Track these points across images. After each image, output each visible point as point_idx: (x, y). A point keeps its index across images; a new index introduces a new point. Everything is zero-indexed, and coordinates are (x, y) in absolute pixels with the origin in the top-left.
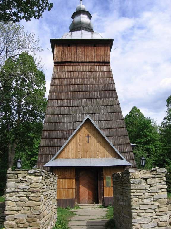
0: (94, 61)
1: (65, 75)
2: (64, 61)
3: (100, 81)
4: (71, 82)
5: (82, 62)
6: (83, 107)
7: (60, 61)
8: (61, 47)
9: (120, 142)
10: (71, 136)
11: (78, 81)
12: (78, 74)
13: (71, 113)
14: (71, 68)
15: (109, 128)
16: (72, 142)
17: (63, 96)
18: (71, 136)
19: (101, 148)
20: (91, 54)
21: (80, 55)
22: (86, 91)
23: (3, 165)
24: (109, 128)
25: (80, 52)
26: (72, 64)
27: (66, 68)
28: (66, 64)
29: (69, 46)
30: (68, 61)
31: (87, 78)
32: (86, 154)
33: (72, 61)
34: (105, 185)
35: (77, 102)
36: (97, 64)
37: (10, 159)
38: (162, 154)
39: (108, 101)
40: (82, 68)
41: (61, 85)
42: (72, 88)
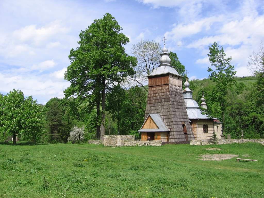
1: (152, 92)
2: (152, 86)
3: (165, 93)
7: (150, 86)
9: (169, 121)
11: (157, 95)
12: (157, 91)
13: (154, 109)
16: (146, 123)
17: (151, 102)
19: (193, 118)
20: (162, 79)
21: (157, 82)
26: (155, 87)
27: (153, 89)
28: (153, 87)
32: (150, 127)
34: (155, 138)
36: (164, 85)
37: (28, 142)
38: (58, 135)
39: (167, 103)
40: (159, 88)
41: (151, 97)
42: (154, 98)
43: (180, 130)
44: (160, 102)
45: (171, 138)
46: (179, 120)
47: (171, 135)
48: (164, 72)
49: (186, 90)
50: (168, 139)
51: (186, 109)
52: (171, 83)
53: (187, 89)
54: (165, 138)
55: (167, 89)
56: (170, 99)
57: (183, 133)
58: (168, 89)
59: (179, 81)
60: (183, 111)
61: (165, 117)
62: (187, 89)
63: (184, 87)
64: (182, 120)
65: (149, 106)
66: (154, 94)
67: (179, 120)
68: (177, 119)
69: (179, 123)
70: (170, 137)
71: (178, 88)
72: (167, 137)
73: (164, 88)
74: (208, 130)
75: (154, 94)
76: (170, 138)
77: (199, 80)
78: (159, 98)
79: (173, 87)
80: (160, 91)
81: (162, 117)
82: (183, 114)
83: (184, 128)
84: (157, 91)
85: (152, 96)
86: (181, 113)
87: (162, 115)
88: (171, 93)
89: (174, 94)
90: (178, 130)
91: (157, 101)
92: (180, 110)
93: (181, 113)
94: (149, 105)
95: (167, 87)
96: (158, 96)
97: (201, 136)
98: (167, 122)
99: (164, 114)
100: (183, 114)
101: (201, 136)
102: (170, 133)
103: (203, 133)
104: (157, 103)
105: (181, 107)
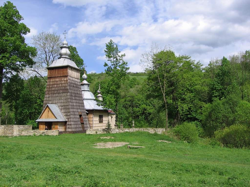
0: (61, 76)
1: (51, 83)
2: (51, 77)
4: (53, 86)
5: (57, 77)
6: (56, 97)
8: (50, 70)
10: (40, 116)
11: (55, 86)
12: (56, 82)
14: (54, 80)
15: (64, 106)
17: (50, 92)
18: (40, 116)
19: (89, 108)
20: (61, 72)
22: (58, 90)
23: (34, 114)
24: (64, 106)
25: (57, 72)
27: (52, 80)
28: (52, 78)
29: (53, 69)
30: (52, 77)
31: (58, 84)
33: (54, 77)
34: (53, 127)
35: (54, 95)
39: (65, 94)
40: (57, 80)
42: (53, 89)
43: (77, 120)
44: (59, 93)
45: (68, 128)
46: (76, 110)
47: (68, 125)
48: (65, 59)
49: (84, 82)
50: (66, 128)
51: (83, 101)
52: (70, 75)
53: (85, 82)
54: (63, 127)
55: (66, 81)
56: (68, 90)
57: (79, 123)
58: (67, 80)
59: (78, 73)
60: (80, 102)
61: (63, 108)
62: (85, 82)
63: (82, 79)
64: (79, 110)
65: (47, 97)
66: (53, 85)
67: (76, 110)
68: (74, 109)
69: (76, 113)
70: (68, 126)
71: (77, 80)
72: (64, 127)
73: (63, 79)
74: (103, 120)
75: (53, 85)
76: (67, 127)
77: (97, 73)
78: (58, 89)
79: (72, 79)
80: (59, 82)
81: (60, 107)
82: (80, 105)
83: (81, 118)
84: (56, 82)
85: (51, 87)
86: (78, 104)
87: (60, 105)
88: (70, 85)
89: (73, 86)
90: (75, 120)
91: (56, 92)
92: (77, 101)
93: (78, 104)
94: (47, 96)
95: (65, 79)
96: (57, 87)
97: (97, 125)
98: (65, 112)
99: (62, 105)
100: (80, 105)
101: (97, 125)
102: (68, 123)
103: (99, 123)
104: (56, 94)
105: (79, 98)
